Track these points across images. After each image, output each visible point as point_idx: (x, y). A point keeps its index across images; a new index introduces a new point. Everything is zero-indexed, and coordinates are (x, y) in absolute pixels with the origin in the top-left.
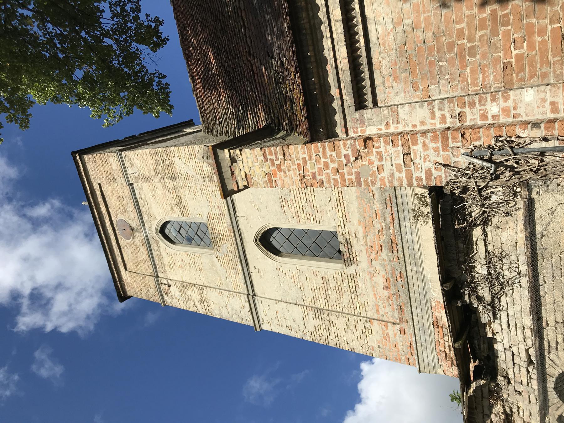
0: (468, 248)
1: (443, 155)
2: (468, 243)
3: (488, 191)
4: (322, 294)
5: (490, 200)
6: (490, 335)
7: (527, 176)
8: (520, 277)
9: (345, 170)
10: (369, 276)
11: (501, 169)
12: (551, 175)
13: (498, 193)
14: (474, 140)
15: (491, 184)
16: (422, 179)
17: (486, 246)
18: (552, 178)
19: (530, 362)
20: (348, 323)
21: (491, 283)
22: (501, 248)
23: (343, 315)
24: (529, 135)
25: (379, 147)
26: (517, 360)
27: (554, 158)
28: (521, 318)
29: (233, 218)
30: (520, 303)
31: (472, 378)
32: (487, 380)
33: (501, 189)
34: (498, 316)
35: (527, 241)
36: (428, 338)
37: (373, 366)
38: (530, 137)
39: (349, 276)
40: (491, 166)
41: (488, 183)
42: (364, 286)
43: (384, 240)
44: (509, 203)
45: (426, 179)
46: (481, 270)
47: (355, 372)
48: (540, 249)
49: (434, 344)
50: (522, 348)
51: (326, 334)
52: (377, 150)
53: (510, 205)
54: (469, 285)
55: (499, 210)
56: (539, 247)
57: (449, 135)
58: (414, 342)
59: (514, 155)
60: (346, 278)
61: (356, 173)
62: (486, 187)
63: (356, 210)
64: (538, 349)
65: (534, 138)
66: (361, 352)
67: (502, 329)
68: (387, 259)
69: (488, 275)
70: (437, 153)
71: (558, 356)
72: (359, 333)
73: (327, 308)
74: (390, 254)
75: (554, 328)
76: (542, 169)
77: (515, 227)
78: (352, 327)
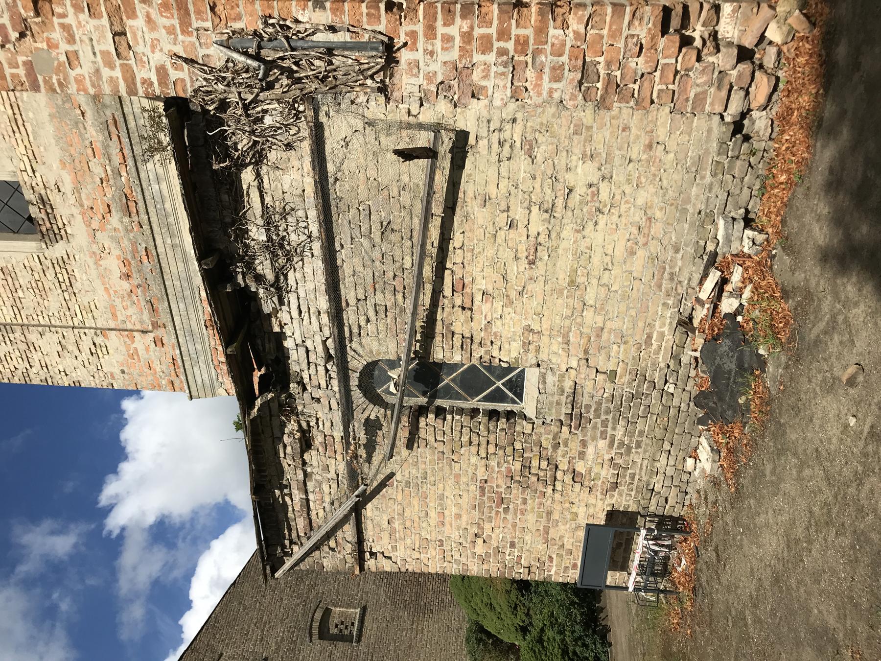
0: (237, 201)
1: (183, 42)
2: (236, 193)
3: (259, 109)
4: (5, 299)
5: (263, 123)
6: (276, 329)
7: (311, 87)
8: (311, 242)
10: (93, 259)
11: (275, 73)
12: (342, 86)
13: (274, 112)
14: (231, 19)
15: (262, 96)
16: (151, 84)
17: (262, 197)
18: (344, 90)
19: (329, 357)
20: (63, 342)
21: (273, 253)
22: (284, 200)
23: (53, 329)
24: (310, 19)
25: (63, 16)
26: (312, 358)
27: (345, 59)
28: (315, 300)
30: (313, 279)
31: (257, 392)
32: (277, 391)
33: (277, 105)
34: (286, 301)
35: (316, 187)
36: (199, 347)
37: (142, 402)
38: (312, 22)
39: (55, 262)
40: (259, 66)
41: (258, 95)
42: (84, 277)
43: (113, 196)
44: (290, 129)
45: (160, 84)
46: (257, 234)
47: (113, 417)
48: (334, 199)
49: (209, 354)
50: (318, 340)
51: (22, 366)
52: (62, 21)
53: (292, 132)
54: (241, 259)
55: (277, 139)
56: (332, 196)
57: (189, 6)
58: (179, 356)
59: (292, 51)
60: (50, 265)
61: (25, 63)
62: (255, 101)
63: (53, 141)
64: (337, 339)
65: (317, 25)
66: (93, 385)
67: (292, 318)
68: (120, 228)
69: (268, 242)
70: (173, 36)
71: (361, 344)
72: (85, 355)
73: (20, 321)
74: (126, 220)
75: (356, 308)
76: (330, 77)
77: (300, 167)
78: (72, 347)
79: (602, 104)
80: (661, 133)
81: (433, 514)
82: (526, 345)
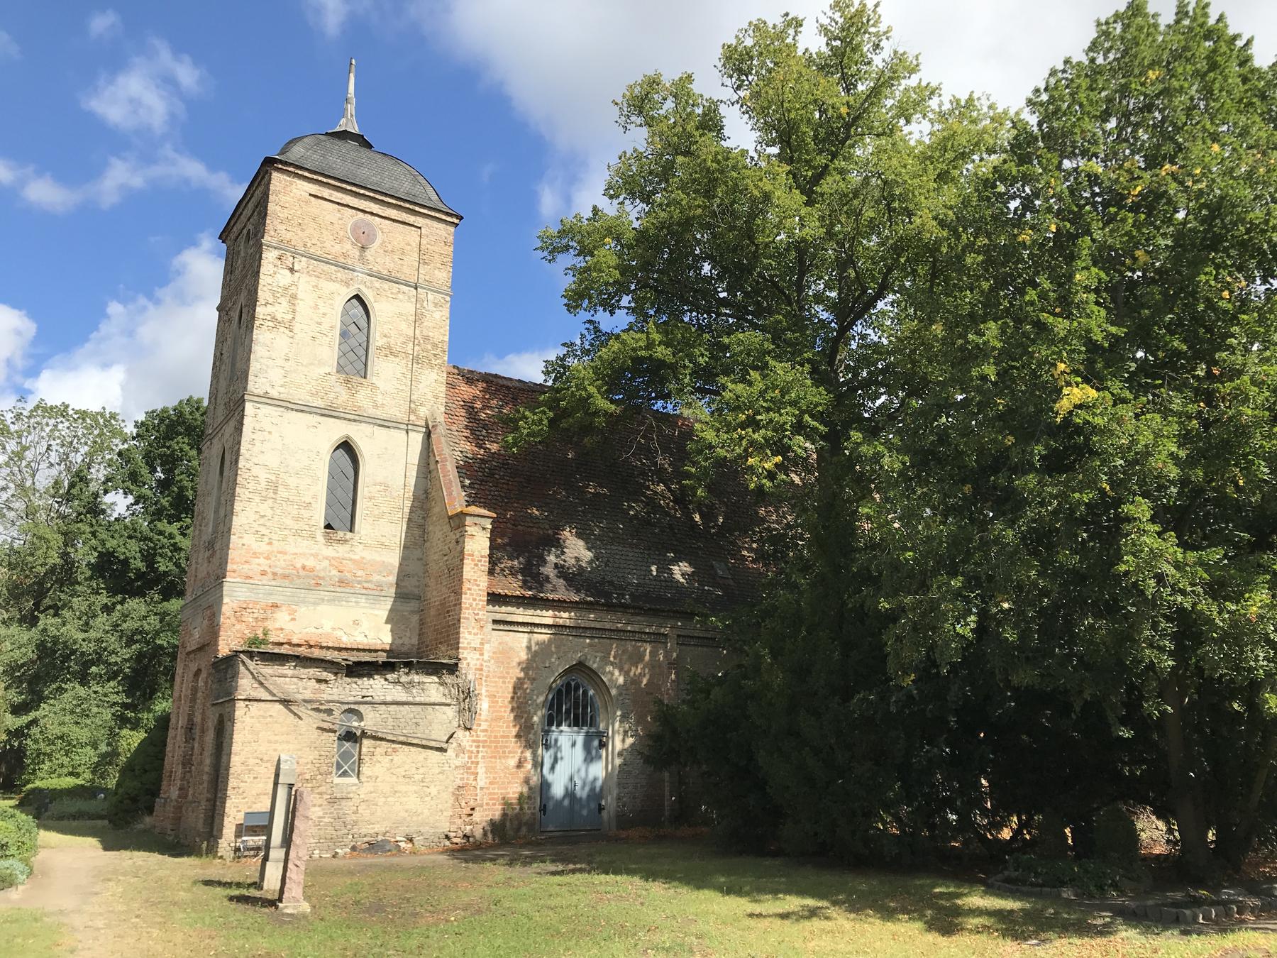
9: (471, 611)
19: (363, 697)
29: (374, 421)
46: (416, 678)
79: (453, 794)
80: (445, 814)
81: (277, 738)
82: (370, 777)
